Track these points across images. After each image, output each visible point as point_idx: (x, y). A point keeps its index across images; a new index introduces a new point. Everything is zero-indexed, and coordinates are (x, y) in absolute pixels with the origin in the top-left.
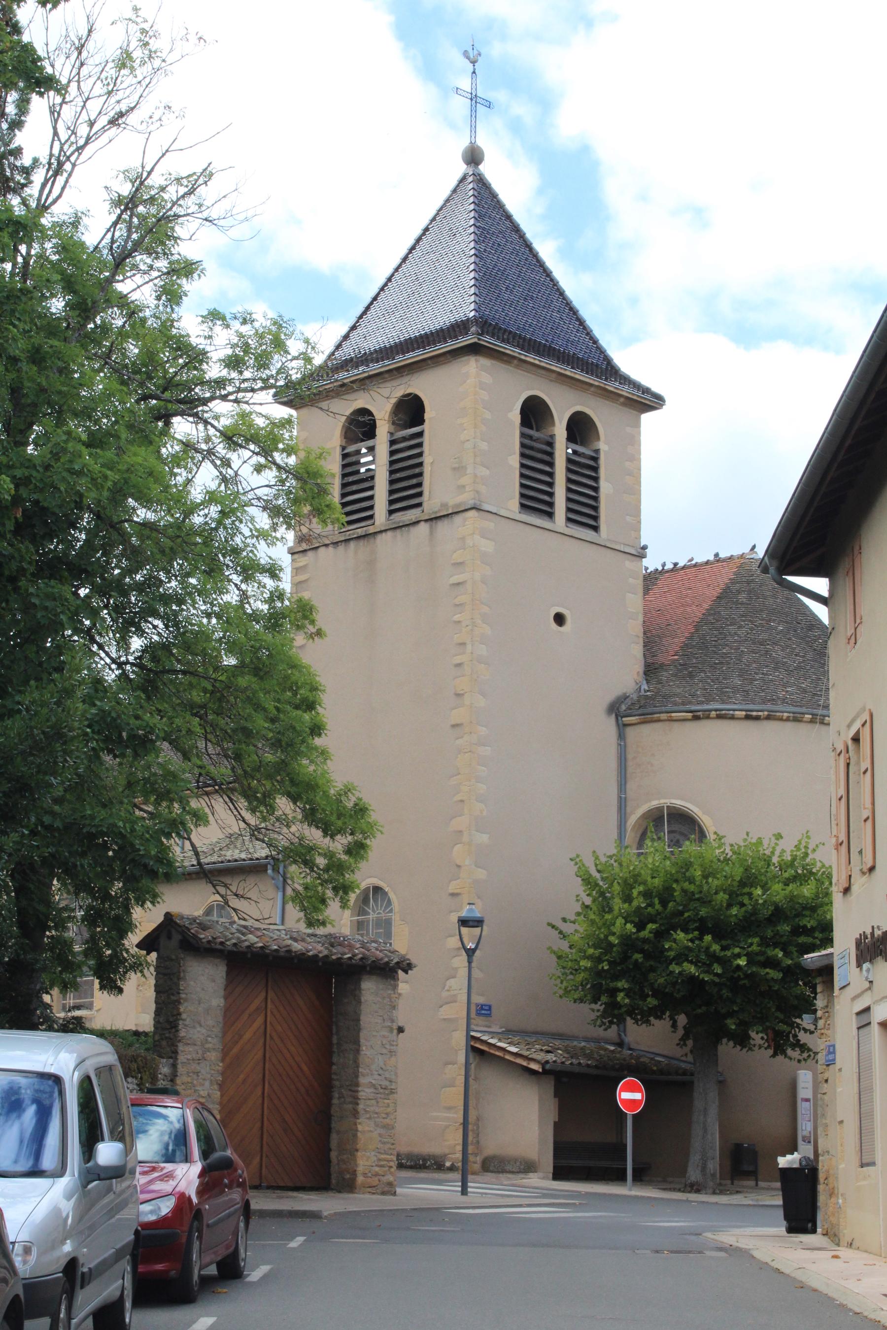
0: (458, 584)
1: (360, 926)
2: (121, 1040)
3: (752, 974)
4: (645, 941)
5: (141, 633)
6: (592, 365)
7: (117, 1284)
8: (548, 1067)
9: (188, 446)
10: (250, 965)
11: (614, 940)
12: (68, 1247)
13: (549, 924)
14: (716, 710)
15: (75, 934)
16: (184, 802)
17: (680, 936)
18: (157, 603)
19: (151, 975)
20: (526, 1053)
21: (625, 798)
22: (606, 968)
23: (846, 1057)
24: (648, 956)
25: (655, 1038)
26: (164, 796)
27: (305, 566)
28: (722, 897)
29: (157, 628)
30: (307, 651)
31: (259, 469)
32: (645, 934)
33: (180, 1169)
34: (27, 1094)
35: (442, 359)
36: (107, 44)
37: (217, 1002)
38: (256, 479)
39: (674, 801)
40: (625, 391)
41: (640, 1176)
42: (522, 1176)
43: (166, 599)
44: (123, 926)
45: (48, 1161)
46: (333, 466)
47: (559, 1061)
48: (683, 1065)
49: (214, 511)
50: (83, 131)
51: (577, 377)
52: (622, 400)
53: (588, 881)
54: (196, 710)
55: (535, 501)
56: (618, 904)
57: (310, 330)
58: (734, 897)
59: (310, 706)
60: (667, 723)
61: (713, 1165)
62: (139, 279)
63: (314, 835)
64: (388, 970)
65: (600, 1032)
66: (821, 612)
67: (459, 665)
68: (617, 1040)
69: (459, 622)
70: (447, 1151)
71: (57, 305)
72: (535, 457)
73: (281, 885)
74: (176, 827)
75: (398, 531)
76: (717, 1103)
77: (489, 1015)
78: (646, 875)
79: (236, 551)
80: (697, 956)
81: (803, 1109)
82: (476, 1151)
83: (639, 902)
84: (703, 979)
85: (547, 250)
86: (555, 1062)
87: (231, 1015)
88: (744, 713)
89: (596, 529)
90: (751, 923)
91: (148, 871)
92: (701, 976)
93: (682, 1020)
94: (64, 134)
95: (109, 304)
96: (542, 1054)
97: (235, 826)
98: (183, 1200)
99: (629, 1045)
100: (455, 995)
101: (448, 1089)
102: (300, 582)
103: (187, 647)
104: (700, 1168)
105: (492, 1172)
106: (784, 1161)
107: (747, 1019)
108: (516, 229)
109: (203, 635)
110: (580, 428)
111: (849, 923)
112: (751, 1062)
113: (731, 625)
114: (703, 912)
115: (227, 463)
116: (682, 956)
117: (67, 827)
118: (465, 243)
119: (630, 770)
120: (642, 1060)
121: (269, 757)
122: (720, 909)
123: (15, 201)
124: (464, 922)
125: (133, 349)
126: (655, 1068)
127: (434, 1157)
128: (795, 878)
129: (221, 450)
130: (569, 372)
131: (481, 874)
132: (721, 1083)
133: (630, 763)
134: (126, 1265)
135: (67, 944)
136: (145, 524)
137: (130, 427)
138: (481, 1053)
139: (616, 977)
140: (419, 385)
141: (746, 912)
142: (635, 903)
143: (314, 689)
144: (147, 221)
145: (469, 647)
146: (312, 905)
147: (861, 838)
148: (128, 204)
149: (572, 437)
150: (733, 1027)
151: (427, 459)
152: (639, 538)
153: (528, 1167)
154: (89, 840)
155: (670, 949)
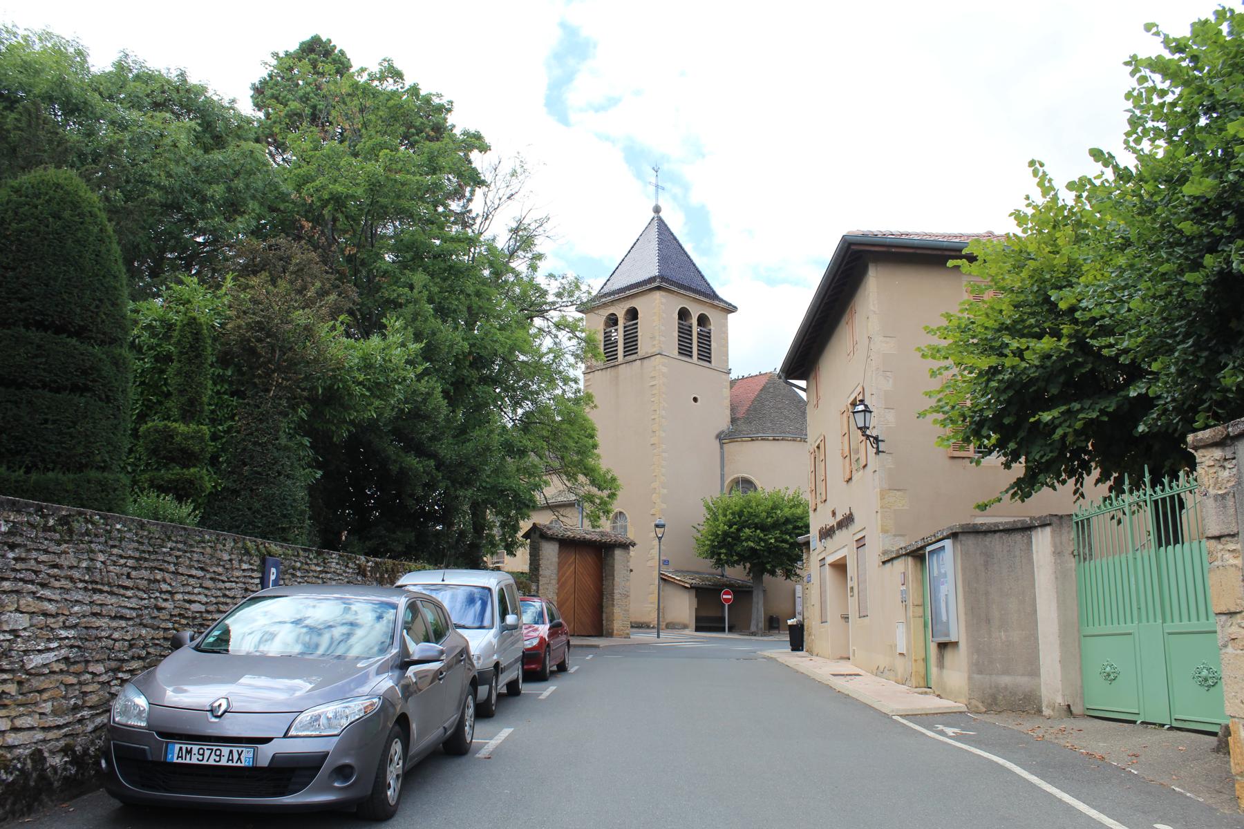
1: (614, 528)
2: (517, 576)
5: (521, 407)
6: (710, 296)
7: (515, 673)
9: (540, 329)
10: (569, 544)
12: (495, 657)
15: (496, 532)
16: (540, 477)
17: (747, 530)
18: (529, 395)
19: (528, 548)
23: (815, 579)
24: (733, 539)
25: (737, 573)
26: (531, 475)
28: (764, 514)
29: (528, 406)
30: (590, 414)
31: (570, 339)
33: (541, 627)
34: (477, 596)
36: (505, 169)
37: (555, 560)
38: (568, 342)
40: (721, 304)
41: (731, 629)
43: (532, 393)
44: (516, 528)
45: (487, 622)
46: (600, 337)
49: (551, 356)
50: (497, 202)
53: (708, 508)
54: (545, 439)
55: (685, 351)
56: (721, 518)
57: (591, 282)
58: (769, 514)
59: (592, 437)
61: (761, 625)
62: (520, 261)
63: (594, 490)
64: (625, 546)
65: (714, 571)
66: (803, 395)
71: (486, 273)
72: (684, 332)
74: (537, 487)
78: (732, 505)
79: (560, 372)
81: (798, 600)
83: (730, 517)
85: (688, 247)
87: (561, 565)
90: (776, 525)
91: (525, 505)
93: (748, 565)
94: (489, 203)
95: (507, 271)
97: (562, 487)
98: (542, 639)
103: (541, 412)
106: (790, 622)
108: (675, 239)
109: (547, 407)
110: (703, 320)
111: (817, 522)
112: (776, 582)
115: (556, 337)
116: (747, 539)
117: (493, 487)
118: (654, 245)
121: (575, 458)
123: (469, 231)
124: (657, 526)
125: (517, 290)
128: (794, 506)
129: (554, 331)
130: (697, 297)
131: (664, 506)
134: (519, 665)
135: (494, 536)
136: (523, 362)
137: (517, 322)
140: (636, 303)
143: (593, 429)
144: (523, 239)
146: (594, 519)
147: (821, 488)
148: (515, 231)
149: (699, 324)
151: (639, 334)
153: (685, 627)
154: (502, 493)
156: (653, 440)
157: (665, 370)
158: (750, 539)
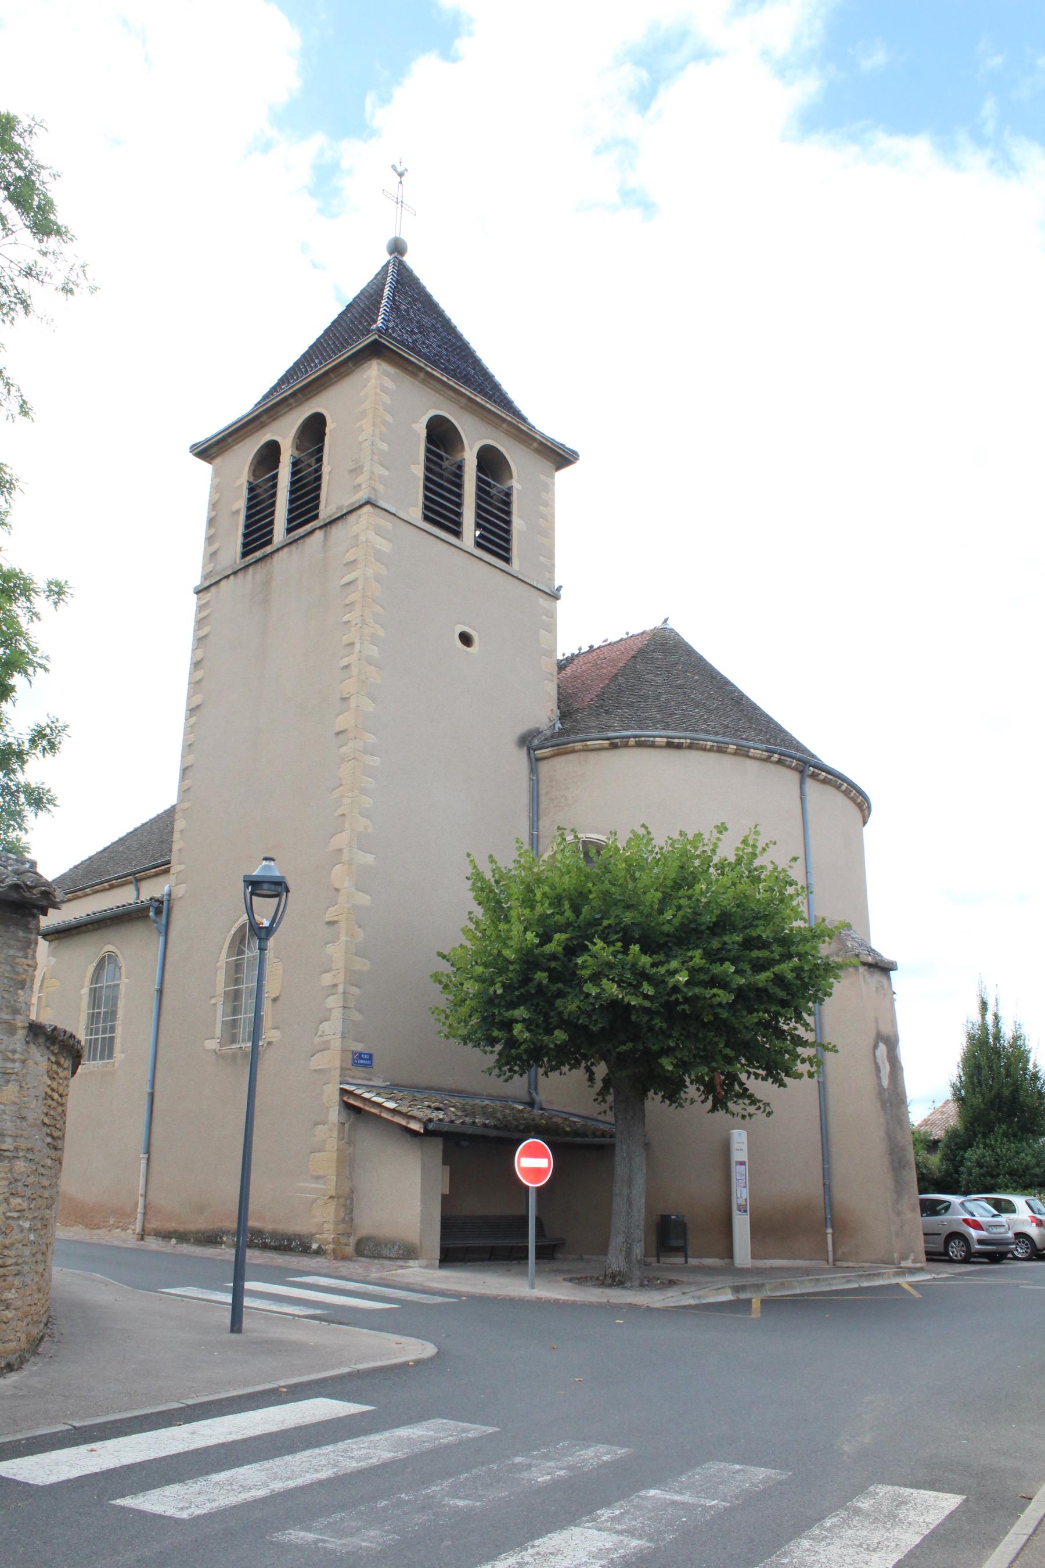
0: (349, 584)
3: (696, 998)
4: (553, 957)
8: (431, 1126)
11: (509, 954)
13: (440, 954)
14: (635, 737)
20: (404, 1109)
21: (538, 836)
22: (499, 992)
25: (568, 1091)
27: (208, 603)
32: (551, 947)
35: (343, 369)
39: (589, 835)
41: (547, 1252)
42: (400, 1263)
47: (447, 1119)
48: (602, 1126)
51: (488, 406)
52: (535, 445)
55: (441, 513)
56: (517, 911)
60: (582, 753)
67: (347, 667)
68: (527, 1099)
69: (349, 622)
70: (313, 1230)
73: (163, 929)
75: (294, 546)
76: (645, 1171)
77: (370, 1066)
80: (622, 975)
82: (348, 1231)
84: (629, 1004)
86: (440, 1120)
88: (665, 740)
89: (507, 560)
90: (688, 934)
92: (626, 1000)
93: (601, 1070)
96: (428, 1111)
99: (540, 1103)
100: (328, 1041)
101: (317, 1154)
102: (203, 618)
104: (623, 1253)
105: (367, 1257)
107: (686, 1059)
110: (491, 463)
112: (685, 1118)
113: (648, 674)
114: (628, 917)
119: (542, 806)
120: (554, 1120)
122: (649, 915)
126: (568, 1129)
127: (298, 1237)
132: (647, 1145)
133: (542, 799)
138: (358, 1110)
139: (513, 1005)
141: (684, 917)
142: (539, 909)
145: (358, 646)
150: (670, 1068)
152: (552, 579)
153: (409, 1253)
155: (584, 967)
156: (343, 721)
157: (383, 545)
158: (605, 975)
